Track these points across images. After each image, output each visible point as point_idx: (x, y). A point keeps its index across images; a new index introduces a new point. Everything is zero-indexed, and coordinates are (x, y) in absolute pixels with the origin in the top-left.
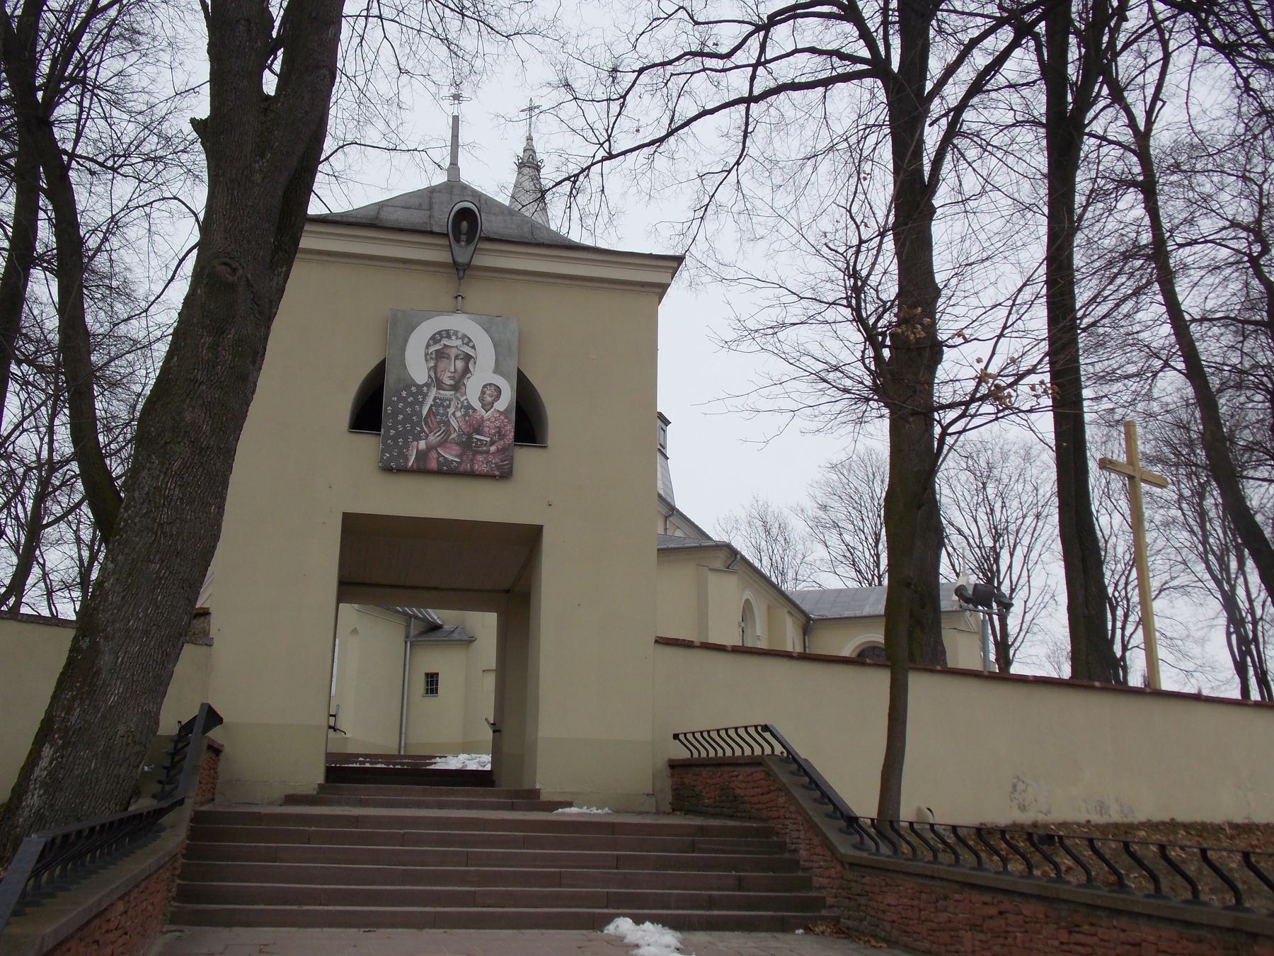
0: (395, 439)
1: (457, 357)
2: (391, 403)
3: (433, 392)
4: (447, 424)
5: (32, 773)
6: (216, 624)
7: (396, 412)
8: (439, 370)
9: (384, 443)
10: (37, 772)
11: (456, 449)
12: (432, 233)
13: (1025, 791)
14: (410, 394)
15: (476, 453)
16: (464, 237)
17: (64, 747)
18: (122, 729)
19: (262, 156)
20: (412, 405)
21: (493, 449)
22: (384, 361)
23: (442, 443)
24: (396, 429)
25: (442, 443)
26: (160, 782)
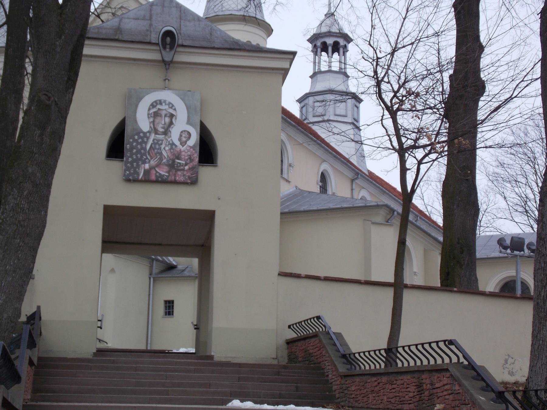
0: (132, 163)
1: (166, 116)
2: (129, 143)
3: (153, 136)
4: (161, 154)
7: (132, 148)
9: (126, 165)
11: (166, 168)
12: (150, 43)
13: (513, 363)
15: (177, 170)
16: (168, 46)
18: (5, 316)
20: (141, 143)
21: (187, 168)
22: (125, 118)
23: (158, 165)
24: (132, 158)
25: (158, 165)
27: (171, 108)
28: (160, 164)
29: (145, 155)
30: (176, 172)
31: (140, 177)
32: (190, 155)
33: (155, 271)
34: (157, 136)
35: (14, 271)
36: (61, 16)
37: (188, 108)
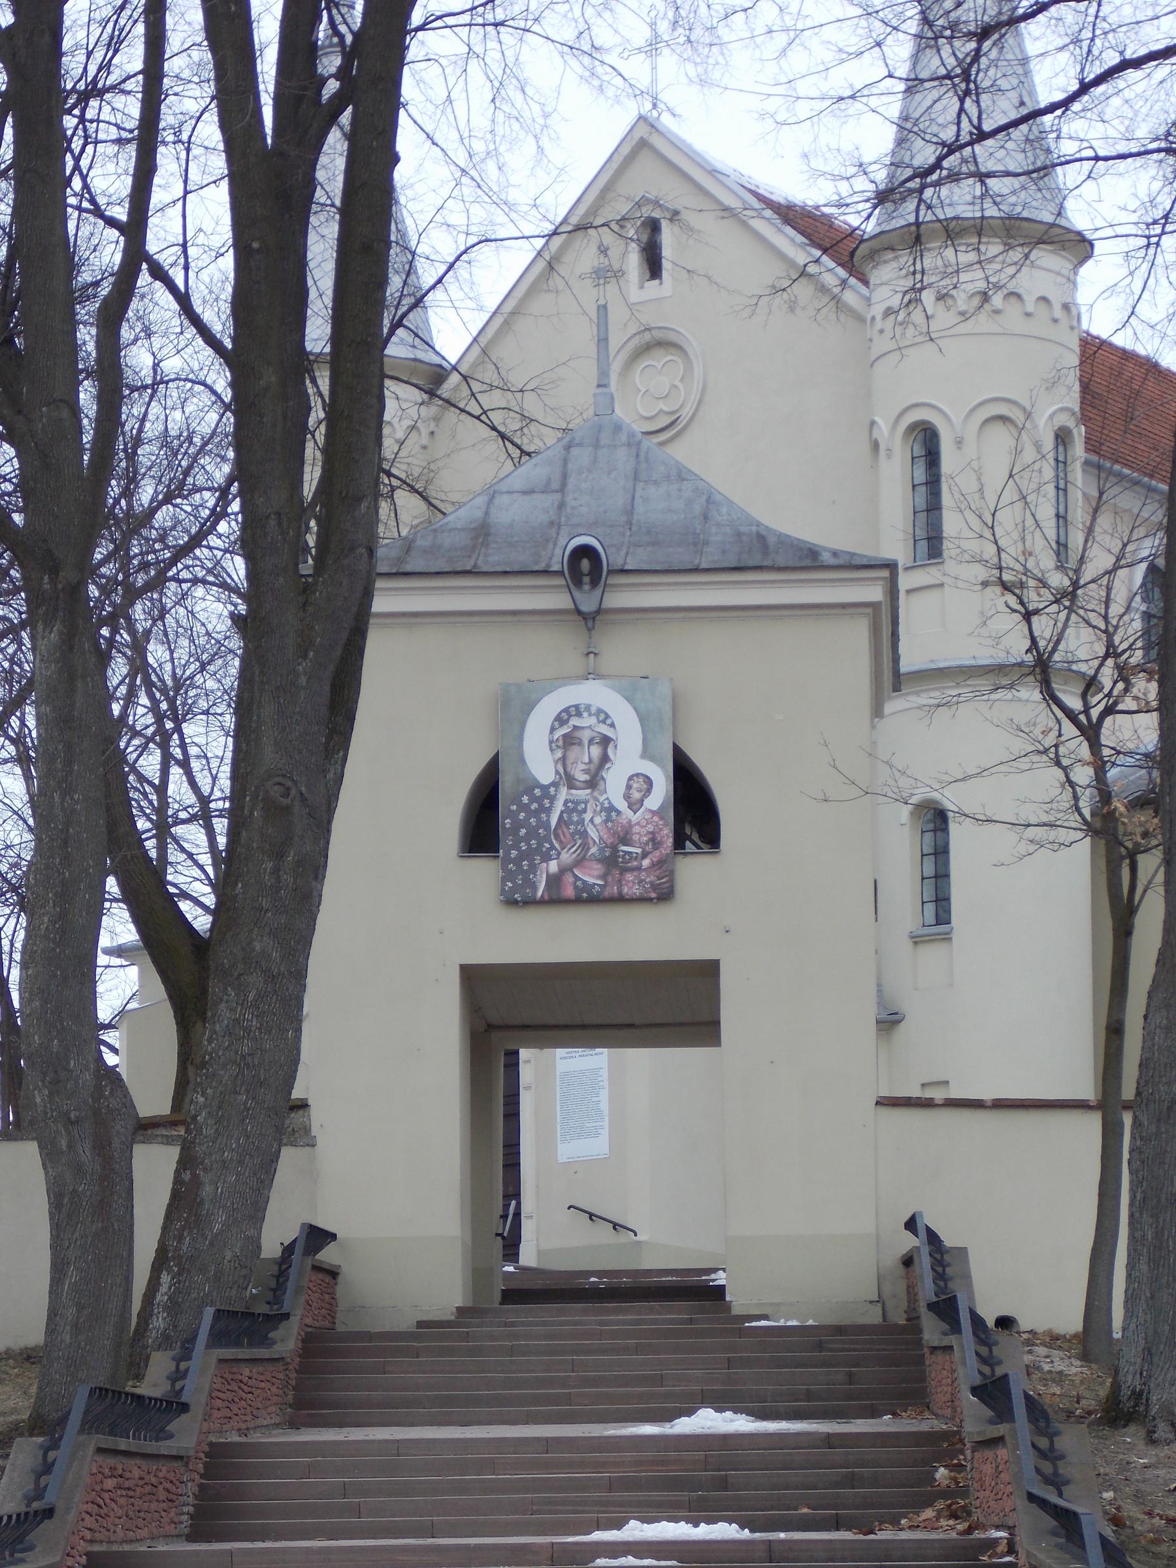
3: (563, 794)
4: (584, 834)
5: (154, 1297)
6: (319, 1118)
8: (569, 762)
9: (504, 868)
10: (158, 1298)
11: (598, 869)
12: (546, 572)
14: (533, 799)
15: (624, 870)
16: (586, 579)
17: (179, 1274)
18: (228, 1255)
19: (305, 657)
20: (536, 813)
21: (646, 863)
23: (579, 862)
24: (519, 849)
25: (579, 862)
26: (269, 1303)
27: (604, 722)
28: (584, 858)
29: (547, 839)
30: (621, 874)
31: (539, 894)
32: (652, 833)
34: (574, 791)
35: (241, 1162)
36: (304, 611)
37: (642, 719)
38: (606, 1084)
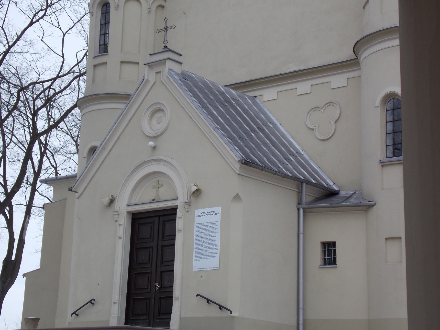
33: (306, 199)
38: (219, 230)
